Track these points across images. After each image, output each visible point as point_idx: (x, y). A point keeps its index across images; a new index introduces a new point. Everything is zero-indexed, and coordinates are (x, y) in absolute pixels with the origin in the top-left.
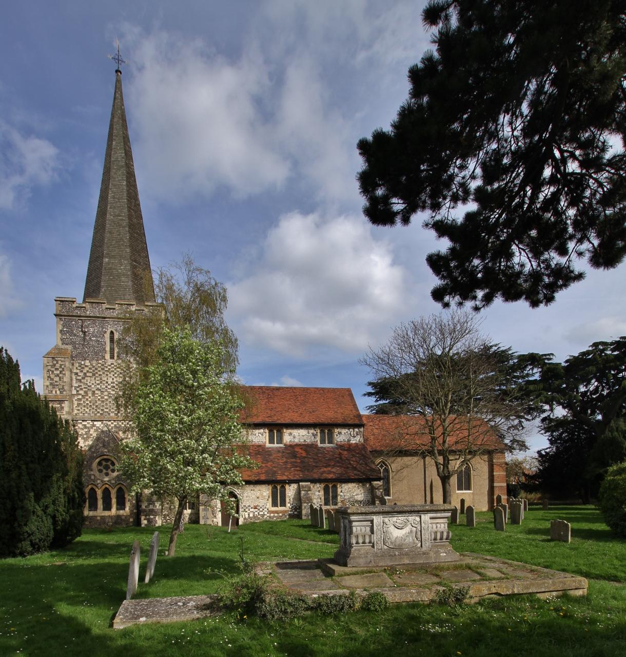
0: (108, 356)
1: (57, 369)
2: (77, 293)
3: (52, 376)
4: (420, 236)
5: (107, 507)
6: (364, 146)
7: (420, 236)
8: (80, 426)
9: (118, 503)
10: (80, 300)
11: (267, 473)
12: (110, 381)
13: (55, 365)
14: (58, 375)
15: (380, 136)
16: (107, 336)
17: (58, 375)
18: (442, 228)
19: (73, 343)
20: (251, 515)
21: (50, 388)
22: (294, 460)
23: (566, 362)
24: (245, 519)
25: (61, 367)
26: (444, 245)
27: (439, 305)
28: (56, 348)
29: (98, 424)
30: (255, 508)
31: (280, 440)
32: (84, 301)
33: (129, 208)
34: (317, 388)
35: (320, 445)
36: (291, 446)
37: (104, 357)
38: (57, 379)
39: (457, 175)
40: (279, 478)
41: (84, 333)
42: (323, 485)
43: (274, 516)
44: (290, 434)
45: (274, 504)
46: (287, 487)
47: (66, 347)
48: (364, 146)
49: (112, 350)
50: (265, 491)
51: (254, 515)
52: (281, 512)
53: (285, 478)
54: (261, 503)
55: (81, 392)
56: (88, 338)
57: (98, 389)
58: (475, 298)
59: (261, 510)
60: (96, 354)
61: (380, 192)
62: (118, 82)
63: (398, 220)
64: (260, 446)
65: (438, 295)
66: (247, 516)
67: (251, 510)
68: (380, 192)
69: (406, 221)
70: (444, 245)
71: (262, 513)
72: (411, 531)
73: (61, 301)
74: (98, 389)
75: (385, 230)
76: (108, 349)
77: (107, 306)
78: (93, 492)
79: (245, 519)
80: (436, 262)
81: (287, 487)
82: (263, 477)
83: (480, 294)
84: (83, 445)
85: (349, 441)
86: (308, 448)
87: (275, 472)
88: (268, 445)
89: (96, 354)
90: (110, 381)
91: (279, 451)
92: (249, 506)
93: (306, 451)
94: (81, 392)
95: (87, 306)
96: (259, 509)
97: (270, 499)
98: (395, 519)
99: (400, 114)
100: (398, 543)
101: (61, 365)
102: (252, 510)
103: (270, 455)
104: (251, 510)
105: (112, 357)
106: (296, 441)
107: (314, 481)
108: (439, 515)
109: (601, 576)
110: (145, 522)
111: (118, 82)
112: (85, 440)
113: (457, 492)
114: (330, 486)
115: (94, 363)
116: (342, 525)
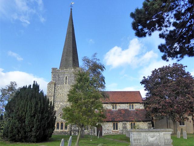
0: (65, 84)
2: (58, 66)
3: (49, 90)
4: (155, 39)
5: (62, 128)
6: (132, 15)
7: (155, 39)
8: (56, 104)
10: (58, 68)
11: (112, 119)
12: (65, 91)
15: (137, 10)
16: (65, 78)
18: (161, 36)
19: (56, 80)
20: (106, 132)
21: (49, 93)
22: (121, 114)
26: (163, 41)
27: (165, 62)
28: (51, 82)
29: (61, 103)
31: (116, 108)
32: (59, 69)
33: (73, 43)
35: (129, 110)
36: (120, 110)
37: (64, 84)
38: (51, 90)
39: (166, 18)
40: (116, 120)
41: (59, 77)
42: (130, 123)
43: (114, 133)
44: (120, 106)
45: (114, 129)
46: (118, 123)
47: (53, 81)
49: (66, 82)
50: (111, 124)
52: (116, 132)
53: (117, 120)
54: (110, 128)
55: (57, 94)
56: (60, 79)
57: (62, 93)
58: (177, 57)
60: (62, 83)
61: (140, 27)
62: (71, 11)
63: (147, 35)
64: (110, 110)
65: (164, 58)
68: (140, 27)
69: (150, 35)
70: (163, 41)
71: (110, 132)
72: (156, 139)
73: (53, 69)
74: (62, 93)
75: (143, 39)
76: (65, 82)
77: (66, 70)
78: (58, 124)
79: (104, 134)
80: (161, 48)
81: (118, 123)
82: (110, 120)
83: (179, 56)
84: (56, 110)
85: (139, 108)
86: (126, 110)
87: (114, 118)
88: (112, 110)
89: (62, 83)
90: (65, 91)
91: (116, 112)
93: (125, 111)
94: (57, 94)
95: (60, 70)
97: (113, 127)
98: (150, 134)
100: (151, 143)
102: (107, 131)
103: (113, 113)
105: (66, 84)
106: (122, 108)
107: (127, 121)
108: (167, 133)
110: (73, 134)
111: (71, 11)
112: (57, 108)
113: (180, 126)
114: (133, 123)
115: (61, 85)
116: (131, 136)
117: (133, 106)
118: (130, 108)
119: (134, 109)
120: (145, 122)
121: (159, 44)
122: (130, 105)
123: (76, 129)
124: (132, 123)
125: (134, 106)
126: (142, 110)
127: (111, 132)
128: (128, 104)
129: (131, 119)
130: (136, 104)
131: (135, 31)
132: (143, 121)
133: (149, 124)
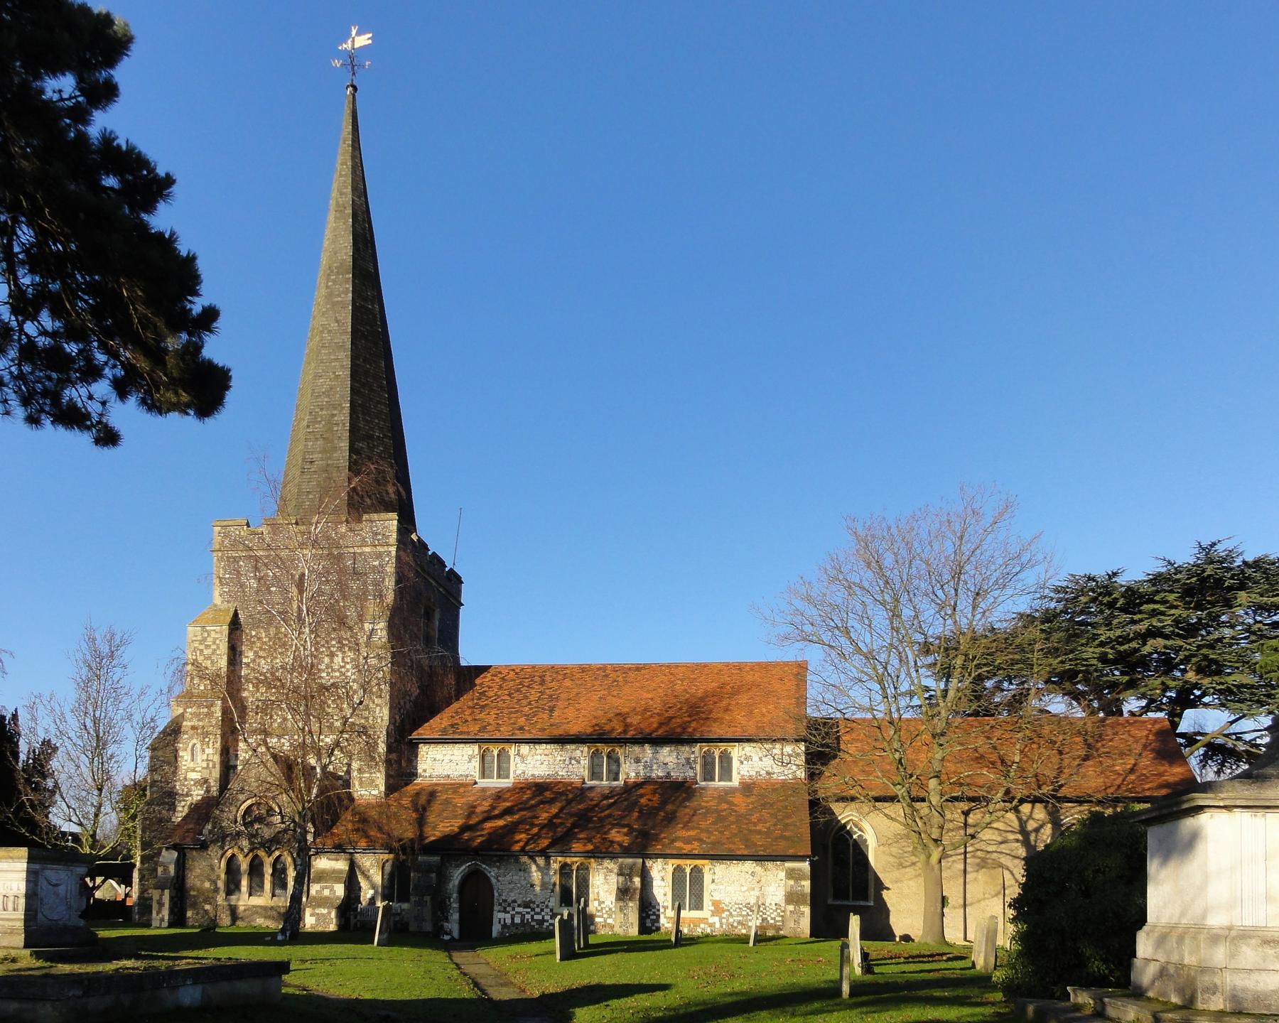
1: (208, 647)
9: (274, 885)
13: (204, 639)
14: (209, 658)
17: (209, 658)
20: (517, 920)
23: (187, 414)
24: (505, 926)
25: (214, 643)
30: (526, 905)
34: (727, 665)
48: (169, 181)
51: (522, 920)
59: (538, 910)
66: (509, 921)
67: (517, 909)
71: (539, 917)
88: (484, 783)
92: (515, 901)
96: (533, 910)
99: (131, 150)
101: (215, 639)
102: (521, 909)
104: (517, 909)
109: (235, 655)
117: (614, 760)
118: (483, 774)
119: (735, 782)
120: (770, 865)
121: (119, 403)
122: (595, 756)
123: (332, 890)
124: (678, 871)
125: (735, 763)
126: (786, 787)
127: (543, 921)
128: (697, 748)
129: (677, 844)
130: (748, 748)
131: (206, 338)
132: (759, 858)
133: (791, 874)
